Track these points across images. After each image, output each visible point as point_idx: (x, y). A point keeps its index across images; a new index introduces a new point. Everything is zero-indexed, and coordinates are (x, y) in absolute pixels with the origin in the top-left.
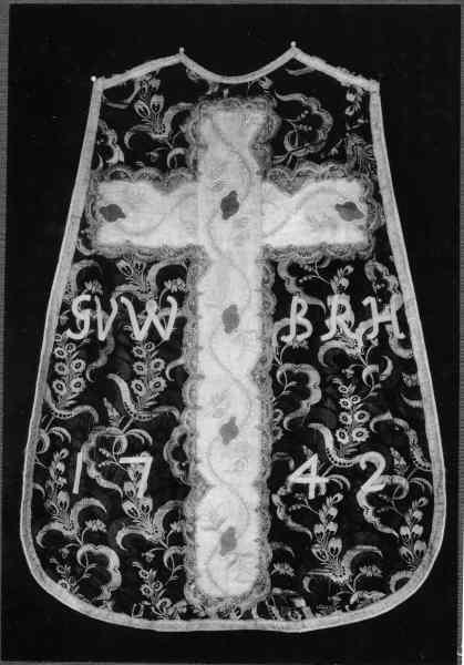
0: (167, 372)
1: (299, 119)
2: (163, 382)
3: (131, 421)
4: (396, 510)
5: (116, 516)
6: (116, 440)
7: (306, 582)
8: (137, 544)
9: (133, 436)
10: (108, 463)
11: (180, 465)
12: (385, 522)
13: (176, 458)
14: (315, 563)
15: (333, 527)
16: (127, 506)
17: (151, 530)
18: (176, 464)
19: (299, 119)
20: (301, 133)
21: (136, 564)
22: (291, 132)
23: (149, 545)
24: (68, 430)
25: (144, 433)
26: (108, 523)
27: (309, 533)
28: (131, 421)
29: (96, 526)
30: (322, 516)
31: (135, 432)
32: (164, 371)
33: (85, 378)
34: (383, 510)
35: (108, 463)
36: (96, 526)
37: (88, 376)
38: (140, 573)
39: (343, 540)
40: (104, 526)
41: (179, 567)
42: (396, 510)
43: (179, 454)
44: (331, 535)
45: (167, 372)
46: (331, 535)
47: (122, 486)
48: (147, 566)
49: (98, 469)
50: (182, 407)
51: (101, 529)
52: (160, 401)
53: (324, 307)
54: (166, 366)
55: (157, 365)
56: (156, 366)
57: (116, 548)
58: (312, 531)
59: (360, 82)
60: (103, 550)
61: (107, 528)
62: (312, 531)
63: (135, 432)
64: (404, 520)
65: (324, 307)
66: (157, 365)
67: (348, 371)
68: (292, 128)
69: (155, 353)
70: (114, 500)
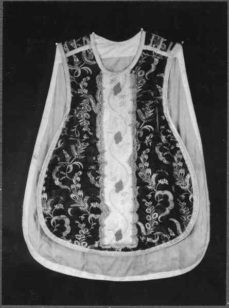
2: (145, 81)
3: (75, 158)
6: (68, 167)
7: (69, 210)
10: (64, 177)
11: (163, 154)
13: (161, 151)
14: (72, 201)
15: (79, 186)
16: (72, 196)
18: (161, 153)
24: (81, 162)
27: (69, 188)
28: (75, 158)
30: (74, 181)
32: (144, 76)
33: (145, 79)
34: (62, 178)
35: (64, 177)
37: (146, 78)
39: (83, 191)
40: (62, 206)
44: (78, 189)
46: (78, 189)
53: (59, 142)
54: (145, 74)
56: (140, 74)
58: (70, 187)
62: (70, 187)
65: (59, 142)
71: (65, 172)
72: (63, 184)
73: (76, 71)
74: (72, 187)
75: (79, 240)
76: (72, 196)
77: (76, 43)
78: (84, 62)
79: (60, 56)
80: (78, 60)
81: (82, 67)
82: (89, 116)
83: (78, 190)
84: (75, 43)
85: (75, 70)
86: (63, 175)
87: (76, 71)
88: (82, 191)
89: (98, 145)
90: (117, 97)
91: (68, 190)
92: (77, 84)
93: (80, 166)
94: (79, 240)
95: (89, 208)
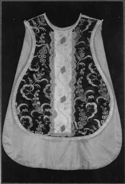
0: (88, 120)
1: (29, 93)
4: (97, 79)
5: (31, 107)
8: (36, 115)
9: (36, 86)
12: (94, 83)
15: (38, 99)
17: (40, 110)
19: (29, 93)
20: (29, 90)
21: (36, 120)
22: (32, 90)
23: (40, 114)
25: (38, 85)
26: (28, 109)
29: (26, 110)
31: (36, 85)
36: (26, 110)
38: (38, 122)
41: (48, 121)
42: (97, 79)
43: (49, 91)
45: (88, 120)
47: (32, 99)
48: (39, 120)
49: (26, 95)
50: (49, 79)
51: (26, 111)
52: (41, 48)
55: (40, 56)
57: (31, 116)
59: (80, 18)
60: (27, 117)
61: (28, 111)
63: (36, 85)
64: (100, 82)
66: (40, 56)
67: (43, 70)
68: (31, 91)
69: (41, 59)
70: (30, 103)
93: (39, 87)
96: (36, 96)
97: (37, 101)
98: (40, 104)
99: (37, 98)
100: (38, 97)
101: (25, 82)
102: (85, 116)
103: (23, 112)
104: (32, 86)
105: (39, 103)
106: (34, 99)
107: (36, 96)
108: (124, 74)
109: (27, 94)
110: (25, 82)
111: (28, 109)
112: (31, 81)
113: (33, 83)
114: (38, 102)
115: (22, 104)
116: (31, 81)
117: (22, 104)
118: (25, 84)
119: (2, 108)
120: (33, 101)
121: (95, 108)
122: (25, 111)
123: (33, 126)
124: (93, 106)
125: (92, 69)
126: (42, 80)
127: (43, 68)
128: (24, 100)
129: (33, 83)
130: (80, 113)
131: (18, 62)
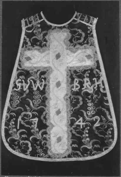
10: (76, 34)
15: (87, 135)
16: (83, 141)
25: (36, 113)
28: (109, 121)
29: (98, 146)
34: (77, 34)
47: (105, 136)
50: (45, 106)
60: (26, 142)
63: (34, 113)
70: (29, 130)
71: (77, 38)
72: (27, 124)
73: (76, 41)
74: (84, 136)
75: (35, 95)
76: (83, 141)
77: (84, 18)
78: (10, 110)
79: (23, 22)
80: (29, 108)
81: (10, 113)
82: (34, 97)
83: (86, 138)
84: (85, 19)
85: (77, 41)
86: (77, 35)
87: (76, 41)
88: (89, 138)
89: (47, 102)
90: (59, 108)
91: (81, 137)
92: (8, 124)
93: (89, 124)
94: (35, 95)
95: (93, 147)
96: (12, 124)
97: (87, 137)
98: (89, 140)
99: (13, 126)
100: (14, 125)
101: (23, 110)
102: (43, 152)
103: (23, 137)
104: (30, 114)
105: (88, 139)
106: (106, 136)
107: (86, 133)
108: (119, 53)
109: (77, 130)
110: (23, 110)
111: (100, 145)
112: (28, 108)
113: (106, 122)
114: (87, 138)
115: (94, 140)
116: (28, 108)
117: (94, 140)
118: (23, 112)
119: (119, 143)
120: (83, 138)
121: (29, 146)
122: (24, 137)
123: (32, 150)
124: (27, 144)
125: (75, 74)
126: (39, 108)
127: (90, 98)
128: (96, 137)
129: (106, 122)
130: (37, 149)
131: (10, 80)
